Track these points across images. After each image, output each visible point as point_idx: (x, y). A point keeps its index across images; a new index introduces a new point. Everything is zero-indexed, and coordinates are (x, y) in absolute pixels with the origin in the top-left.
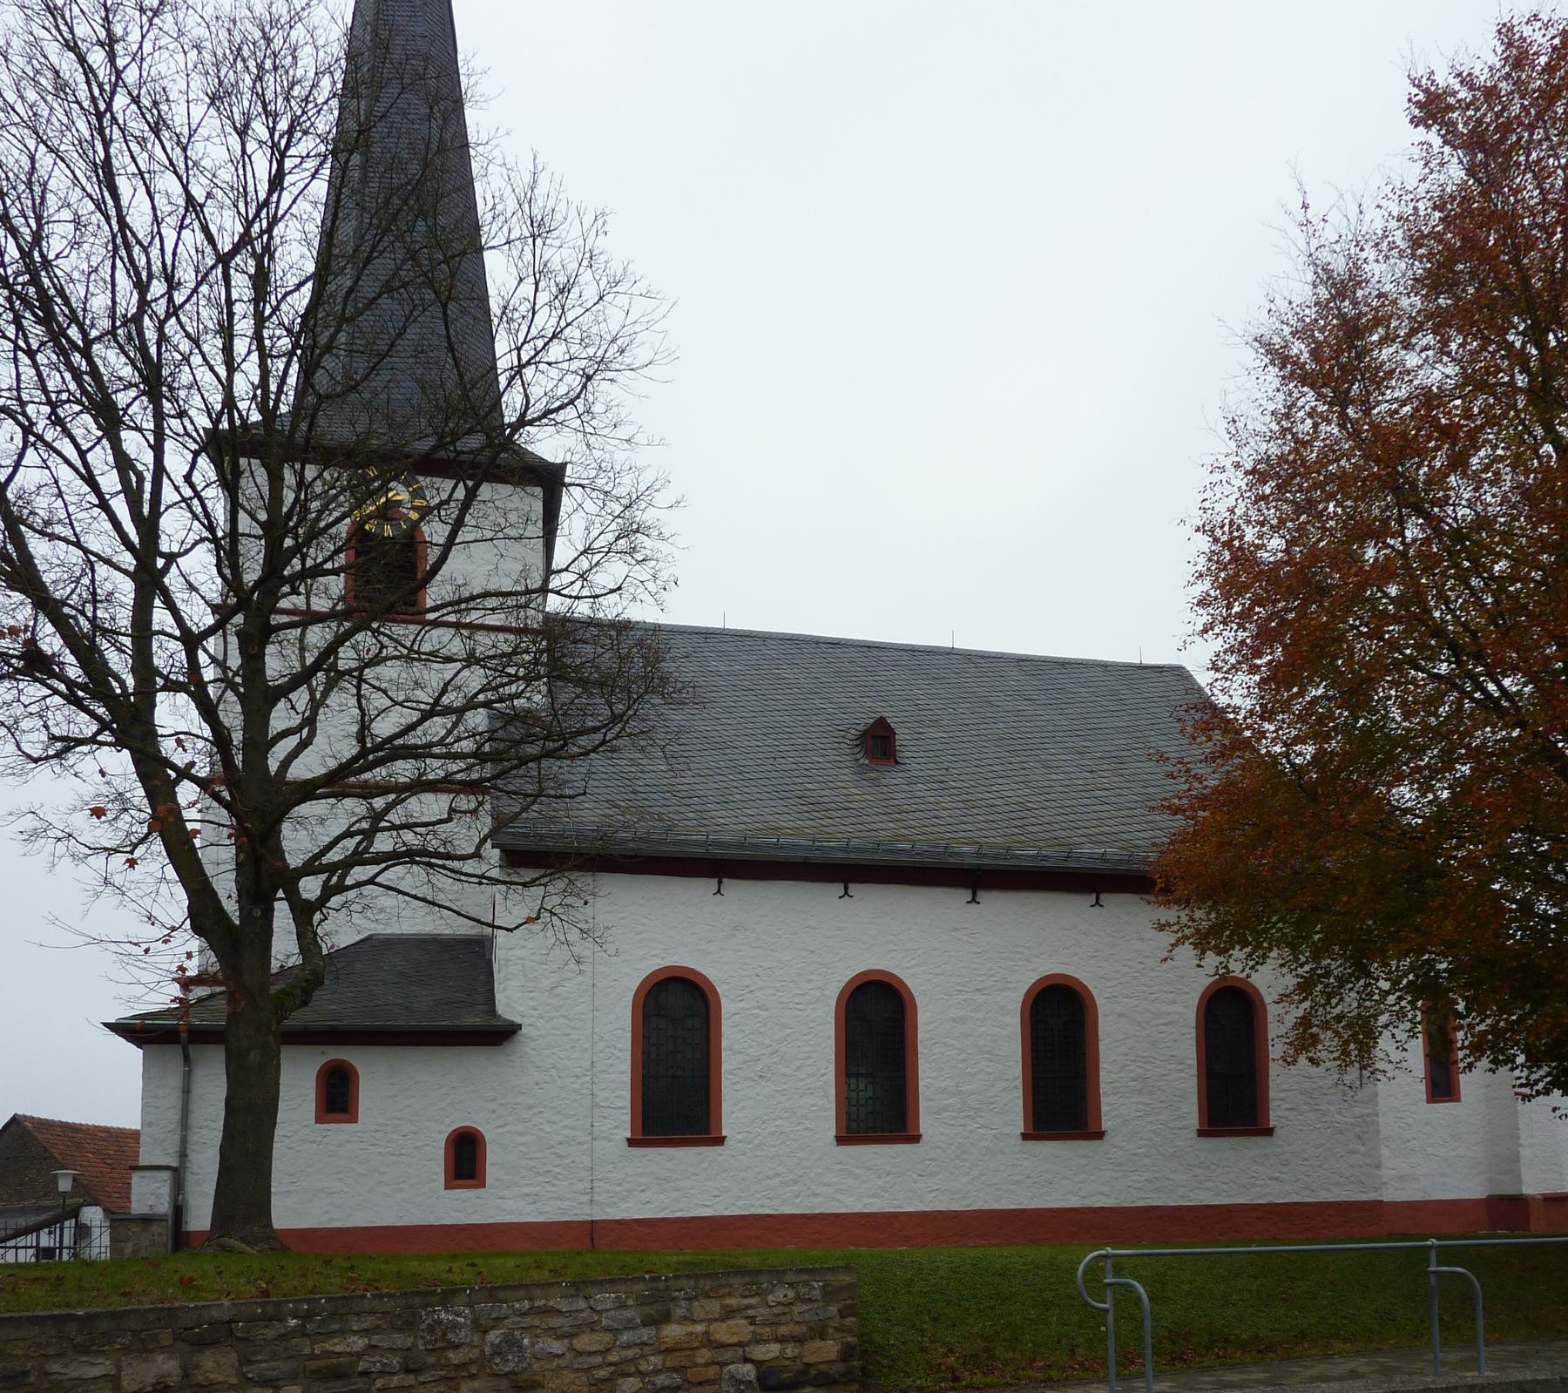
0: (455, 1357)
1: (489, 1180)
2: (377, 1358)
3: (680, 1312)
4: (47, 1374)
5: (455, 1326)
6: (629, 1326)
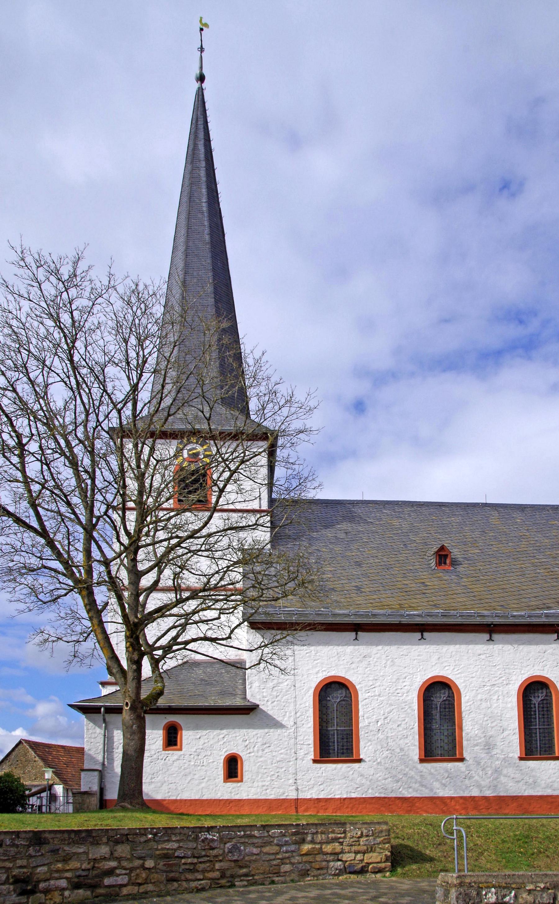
0: (215, 852)
1: (246, 776)
2: (182, 851)
3: (309, 838)
4: (65, 850)
5: (213, 840)
6: (286, 843)
